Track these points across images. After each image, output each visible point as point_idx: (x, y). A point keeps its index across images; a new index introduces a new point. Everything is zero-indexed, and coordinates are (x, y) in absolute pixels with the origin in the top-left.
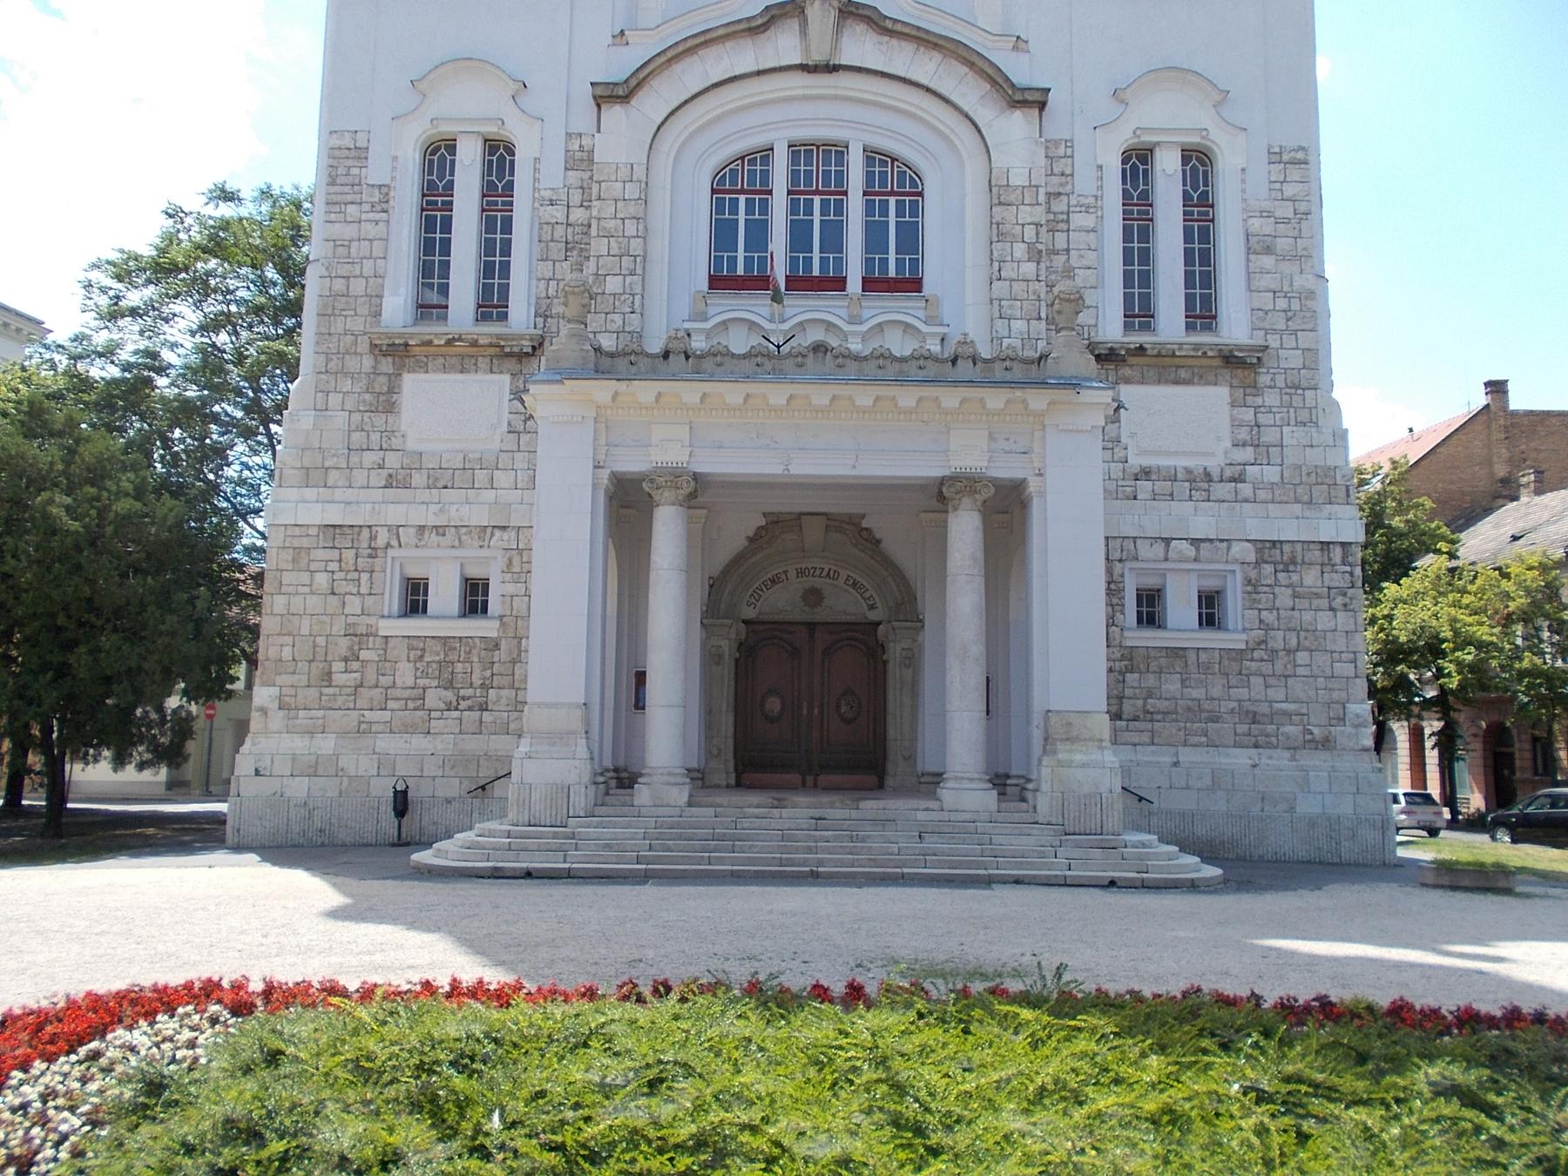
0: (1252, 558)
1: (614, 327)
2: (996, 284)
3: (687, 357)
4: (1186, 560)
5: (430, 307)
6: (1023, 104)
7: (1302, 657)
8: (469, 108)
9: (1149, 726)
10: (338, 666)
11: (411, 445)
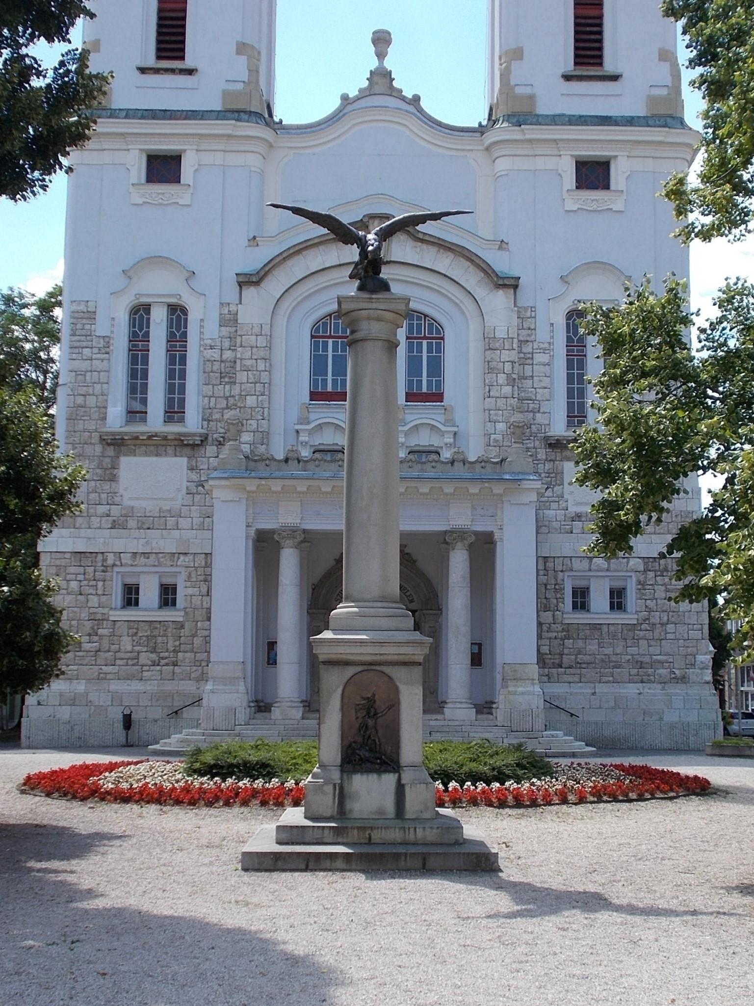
0: (641, 568)
2: (488, 400)
3: (299, 462)
4: (602, 571)
5: (136, 414)
6: (504, 286)
7: (670, 628)
8: (159, 286)
9: (578, 671)
11: (127, 502)
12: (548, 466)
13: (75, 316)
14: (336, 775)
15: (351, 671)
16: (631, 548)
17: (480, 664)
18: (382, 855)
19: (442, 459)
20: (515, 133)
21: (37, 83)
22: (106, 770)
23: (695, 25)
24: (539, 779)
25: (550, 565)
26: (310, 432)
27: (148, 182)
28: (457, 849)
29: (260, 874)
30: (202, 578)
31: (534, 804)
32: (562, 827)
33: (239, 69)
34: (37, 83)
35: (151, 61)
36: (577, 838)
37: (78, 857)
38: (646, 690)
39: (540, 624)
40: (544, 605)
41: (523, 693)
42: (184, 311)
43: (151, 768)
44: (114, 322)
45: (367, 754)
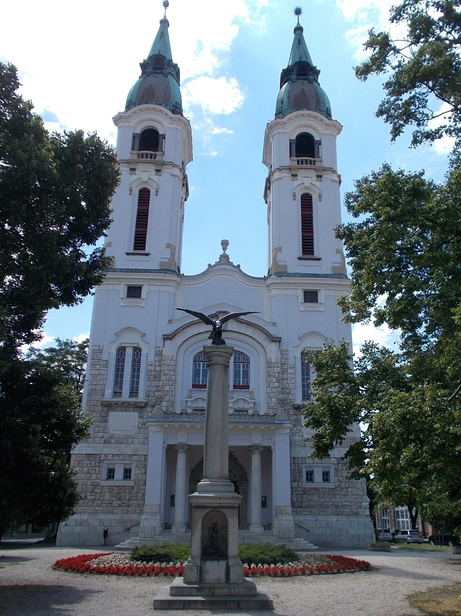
0: (336, 462)
1: (167, 400)
2: (268, 389)
4: (319, 463)
5: (117, 393)
7: (350, 489)
8: (130, 339)
10: (88, 494)
11: (111, 432)
12: (294, 417)
13: (94, 351)
14: (198, 562)
15: (206, 511)
16: (329, 455)
17: (266, 506)
18: (219, 601)
19: (249, 414)
20: (279, 280)
21: (82, 260)
22: (94, 558)
23: (348, 242)
24: (292, 563)
25: (296, 461)
26: (192, 402)
27: (128, 296)
28: (253, 599)
29: (161, 611)
30: (143, 466)
31: (290, 575)
32: (303, 587)
33: (167, 254)
34: (82, 260)
35: (131, 250)
36: (310, 592)
37: (76, 602)
38: (340, 519)
39: (292, 488)
40: (294, 479)
41: (285, 521)
42: (140, 350)
43: (115, 557)
44: (110, 354)
45: (213, 551)
